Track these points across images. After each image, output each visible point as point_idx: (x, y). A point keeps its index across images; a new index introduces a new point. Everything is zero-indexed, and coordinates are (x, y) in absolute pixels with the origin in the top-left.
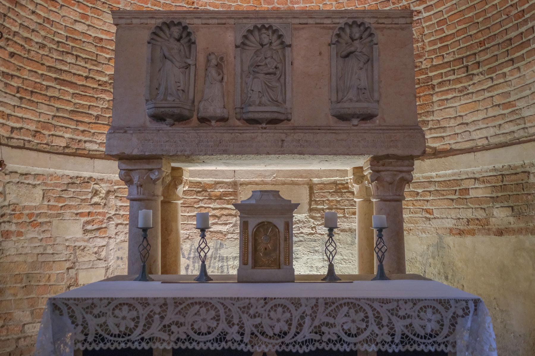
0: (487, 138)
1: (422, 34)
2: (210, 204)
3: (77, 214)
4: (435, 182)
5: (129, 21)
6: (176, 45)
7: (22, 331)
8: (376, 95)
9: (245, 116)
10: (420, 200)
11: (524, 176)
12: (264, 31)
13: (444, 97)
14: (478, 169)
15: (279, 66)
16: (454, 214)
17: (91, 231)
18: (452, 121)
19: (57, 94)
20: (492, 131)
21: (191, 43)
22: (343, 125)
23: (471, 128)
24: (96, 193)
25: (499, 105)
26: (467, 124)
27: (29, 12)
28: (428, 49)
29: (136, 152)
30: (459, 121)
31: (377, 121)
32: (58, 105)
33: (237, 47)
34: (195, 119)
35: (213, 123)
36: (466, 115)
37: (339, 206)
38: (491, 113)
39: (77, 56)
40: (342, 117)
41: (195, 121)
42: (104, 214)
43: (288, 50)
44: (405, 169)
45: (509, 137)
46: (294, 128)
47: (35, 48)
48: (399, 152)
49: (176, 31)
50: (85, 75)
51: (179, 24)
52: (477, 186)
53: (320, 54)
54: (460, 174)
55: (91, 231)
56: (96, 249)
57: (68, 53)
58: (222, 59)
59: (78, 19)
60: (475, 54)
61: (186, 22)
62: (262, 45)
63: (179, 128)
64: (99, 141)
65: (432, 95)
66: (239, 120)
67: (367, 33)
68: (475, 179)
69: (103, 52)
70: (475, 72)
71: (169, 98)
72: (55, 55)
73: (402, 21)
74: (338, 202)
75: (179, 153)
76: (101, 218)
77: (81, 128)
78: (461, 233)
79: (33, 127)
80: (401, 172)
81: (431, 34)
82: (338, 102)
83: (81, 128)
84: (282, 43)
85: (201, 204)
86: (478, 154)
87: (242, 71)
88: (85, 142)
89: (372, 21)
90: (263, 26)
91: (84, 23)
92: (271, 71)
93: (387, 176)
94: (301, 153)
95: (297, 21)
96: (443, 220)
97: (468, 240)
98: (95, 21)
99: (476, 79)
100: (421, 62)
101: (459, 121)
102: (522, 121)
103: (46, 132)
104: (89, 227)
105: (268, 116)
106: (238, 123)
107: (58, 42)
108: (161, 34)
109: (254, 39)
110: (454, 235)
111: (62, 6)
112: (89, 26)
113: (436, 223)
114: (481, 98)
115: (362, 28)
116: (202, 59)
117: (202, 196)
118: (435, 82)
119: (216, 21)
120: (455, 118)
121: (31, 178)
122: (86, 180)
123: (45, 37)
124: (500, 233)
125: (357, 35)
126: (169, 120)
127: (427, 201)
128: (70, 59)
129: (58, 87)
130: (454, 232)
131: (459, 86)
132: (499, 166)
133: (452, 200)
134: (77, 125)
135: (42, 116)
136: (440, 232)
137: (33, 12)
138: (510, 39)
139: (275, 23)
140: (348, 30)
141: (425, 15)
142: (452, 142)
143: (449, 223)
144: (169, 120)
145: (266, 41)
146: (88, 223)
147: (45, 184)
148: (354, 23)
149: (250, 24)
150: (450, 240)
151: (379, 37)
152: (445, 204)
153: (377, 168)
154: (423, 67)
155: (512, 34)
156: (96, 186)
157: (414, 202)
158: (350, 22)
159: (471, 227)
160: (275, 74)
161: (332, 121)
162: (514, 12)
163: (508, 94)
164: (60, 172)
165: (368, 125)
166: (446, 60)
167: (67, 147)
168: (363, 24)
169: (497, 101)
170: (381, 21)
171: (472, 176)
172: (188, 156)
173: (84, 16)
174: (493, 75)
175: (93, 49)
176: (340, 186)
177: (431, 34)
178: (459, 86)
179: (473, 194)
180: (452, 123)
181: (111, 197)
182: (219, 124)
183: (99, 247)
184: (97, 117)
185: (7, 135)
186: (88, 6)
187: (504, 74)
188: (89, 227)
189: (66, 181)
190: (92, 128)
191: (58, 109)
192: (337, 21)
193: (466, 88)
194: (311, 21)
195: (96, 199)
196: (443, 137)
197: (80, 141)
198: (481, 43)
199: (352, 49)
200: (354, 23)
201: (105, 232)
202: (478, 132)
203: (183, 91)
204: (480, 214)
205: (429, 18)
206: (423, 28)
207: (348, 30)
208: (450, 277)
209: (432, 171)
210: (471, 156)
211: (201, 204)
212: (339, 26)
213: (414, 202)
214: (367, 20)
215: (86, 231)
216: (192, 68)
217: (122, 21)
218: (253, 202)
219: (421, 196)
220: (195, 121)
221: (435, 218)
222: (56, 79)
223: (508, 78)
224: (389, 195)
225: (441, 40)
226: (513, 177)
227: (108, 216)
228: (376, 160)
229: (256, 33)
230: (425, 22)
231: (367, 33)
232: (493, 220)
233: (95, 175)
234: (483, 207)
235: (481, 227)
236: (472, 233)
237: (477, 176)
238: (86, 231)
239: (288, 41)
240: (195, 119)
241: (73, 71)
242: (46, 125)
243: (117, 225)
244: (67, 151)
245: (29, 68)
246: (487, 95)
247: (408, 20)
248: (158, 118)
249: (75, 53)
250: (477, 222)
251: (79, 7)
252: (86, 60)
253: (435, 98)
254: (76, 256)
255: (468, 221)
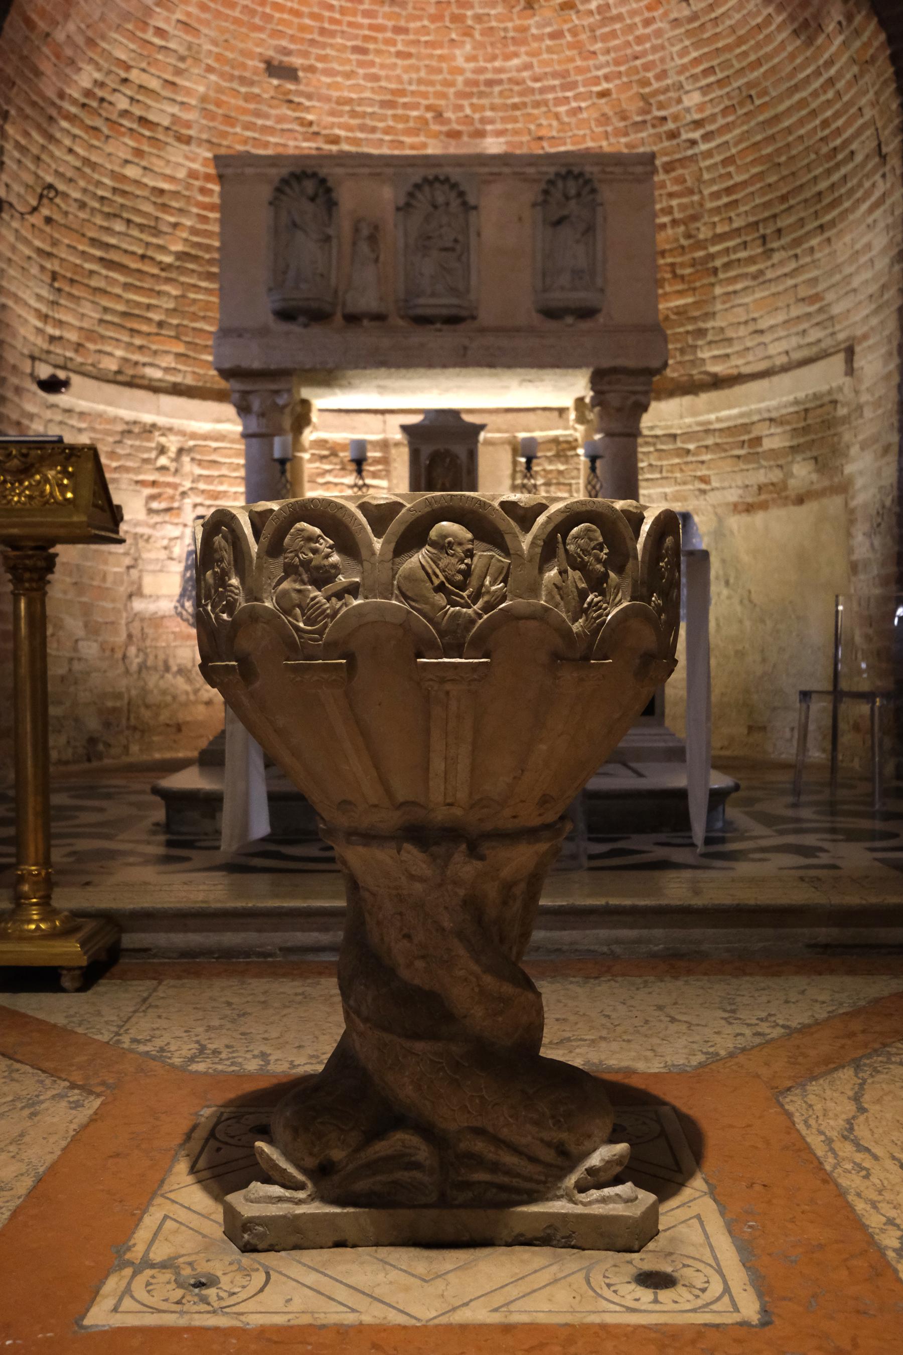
0: (787, 353)
1: (699, 179)
2: (343, 477)
3: (137, 482)
4: (715, 430)
5: (239, 171)
6: (309, 207)
7: (75, 649)
8: (599, 282)
9: (412, 312)
10: (692, 462)
11: (829, 408)
12: (437, 185)
13: (730, 288)
14: (773, 403)
15: (460, 238)
16: (739, 480)
17: (157, 512)
18: (742, 327)
19: (102, 284)
20: (794, 341)
21: (331, 205)
22: (552, 325)
23: (767, 338)
24: (162, 450)
25: (803, 300)
26: (762, 332)
27: (65, 150)
28: (709, 205)
29: (256, 365)
30: (751, 327)
31: (601, 319)
32: (105, 302)
33: (398, 209)
34: (338, 317)
35: (365, 322)
36: (762, 317)
37: (562, 480)
38: (795, 312)
39: (129, 221)
40: (551, 313)
41: (338, 318)
42: (175, 486)
43: (473, 214)
44: (639, 388)
45: (815, 349)
46: (483, 330)
47: (73, 208)
48: (631, 363)
49: (310, 186)
50: (140, 251)
51: (314, 175)
52: (772, 431)
53: (520, 219)
54: (749, 414)
55: (157, 512)
56: (165, 542)
57: (115, 216)
58: (376, 228)
59: (129, 157)
60: (775, 216)
61: (323, 172)
62: (435, 207)
63: (316, 331)
64: (164, 365)
65: (713, 285)
66: (402, 317)
67: (587, 189)
68: (771, 420)
69: (164, 212)
70: (775, 245)
71: (303, 286)
72: (99, 220)
73: (639, 169)
74: (560, 472)
75: (318, 366)
76: (170, 491)
77: (138, 341)
78: (749, 508)
79: (72, 336)
80: (634, 393)
81: (713, 181)
82: (545, 290)
83: (138, 341)
84: (464, 204)
85: (329, 478)
86: (775, 379)
87: (407, 246)
88: (144, 365)
89: (596, 169)
90: (437, 178)
91: (137, 165)
92: (449, 244)
93: (614, 399)
94: (491, 365)
95: (486, 170)
96: (725, 492)
97: (759, 518)
98: (154, 160)
99: (777, 257)
100: (698, 229)
101: (751, 327)
102: (829, 323)
103: (91, 346)
104: (155, 505)
105: (445, 312)
106: (401, 322)
107: (102, 198)
108: (287, 190)
109: (423, 198)
110: (740, 512)
111: (108, 137)
112: (145, 168)
113: (713, 498)
114: (781, 288)
115: (581, 181)
116: (347, 227)
117: (331, 463)
118: (718, 263)
119: (366, 170)
120: (746, 323)
121: (76, 416)
122: (148, 428)
123: (85, 191)
124: (800, 500)
125: (573, 192)
126: (302, 319)
127: (703, 462)
128: (119, 227)
129: (104, 272)
130: (740, 508)
131: (753, 269)
132: (801, 395)
133: (738, 457)
134: (132, 336)
135: (86, 319)
136: (719, 511)
137: (71, 151)
138: (820, 194)
139: (455, 174)
140: (560, 184)
141: (704, 147)
142: (740, 362)
143: (733, 496)
144: (302, 319)
145: (441, 199)
146: (153, 497)
147: (93, 429)
148: (570, 172)
149: (416, 175)
150: (735, 522)
151: (607, 194)
152: (727, 466)
153: (599, 387)
154: (701, 236)
155: (823, 185)
156: (163, 440)
157: (683, 467)
158: (563, 171)
159: (763, 497)
160: (453, 250)
161: (536, 319)
162: (825, 150)
163: (814, 281)
164: (112, 411)
165: (585, 325)
166: (735, 225)
167: (119, 372)
168: (581, 174)
169: (803, 292)
170: (609, 169)
171: (766, 415)
172: (330, 372)
173: (139, 153)
174: (798, 251)
175: (148, 208)
176: (565, 446)
177: (713, 181)
178: (753, 269)
179: (767, 444)
180: (742, 331)
181: (186, 459)
182: (373, 324)
183: (171, 539)
184: (160, 324)
185: (45, 346)
186: (143, 135)
187: (812, 249)
188: (155, 505)
189: (120, 427)
190: (153, 342)
191: (106, 310)
192: (544, 169)
193: (761, 272)
194: (506, 170)
195: (163, 461)
196: (727, 356)
197: (136, 363)
198: (784, 198)
199: (566, 212)
200: (570, 172)
201: (178, 515)
202: (776, 343)
203: (322, 275)
204: (776, 476)
205: (708, 154)
206: (700, 169)
207: (560, 184)
208: (732, 581)
209: (710, 411)
210: (764, 383)
211: (329, 478)
212: (547, 177)
213: (683, 467)
214: (588, 169)
215: (150, 511)
216: (334, 242)
217: (229, 171)
218: (427, 422)
219: (694, 455)
220: (338, 318)
221: (713, 490)
222: (101, 259)
223: (818, 255)
224: (616, 426)
225: (728, 191)
226: (819, 411)
227: (181, 489)
228: (598, 379)
229: (427, 189)
230: (704, 159)
231: (587, 189)
232: (792, 482)
233: (161, 421)
234: (779, 463)
235: (775, 496)
236: (763, 506)
237: (774, 415)
238: (150, 511)
239: (472, 200)
240: (338, 317)
241: (125, 246)
242: (90, 334)
243: (195, 506)
244: (120, 378)
245: (66, 241)
246: (790, 282)
247: (649, 168)
248: (286, 315)
249: (125, 215)
250: (771, 488)
251: (131, 138)
252: (141, 227)
253: (718, 291)
254: (138, 550)
255: (760, 488)
